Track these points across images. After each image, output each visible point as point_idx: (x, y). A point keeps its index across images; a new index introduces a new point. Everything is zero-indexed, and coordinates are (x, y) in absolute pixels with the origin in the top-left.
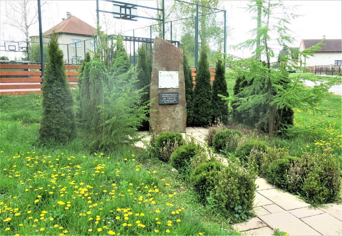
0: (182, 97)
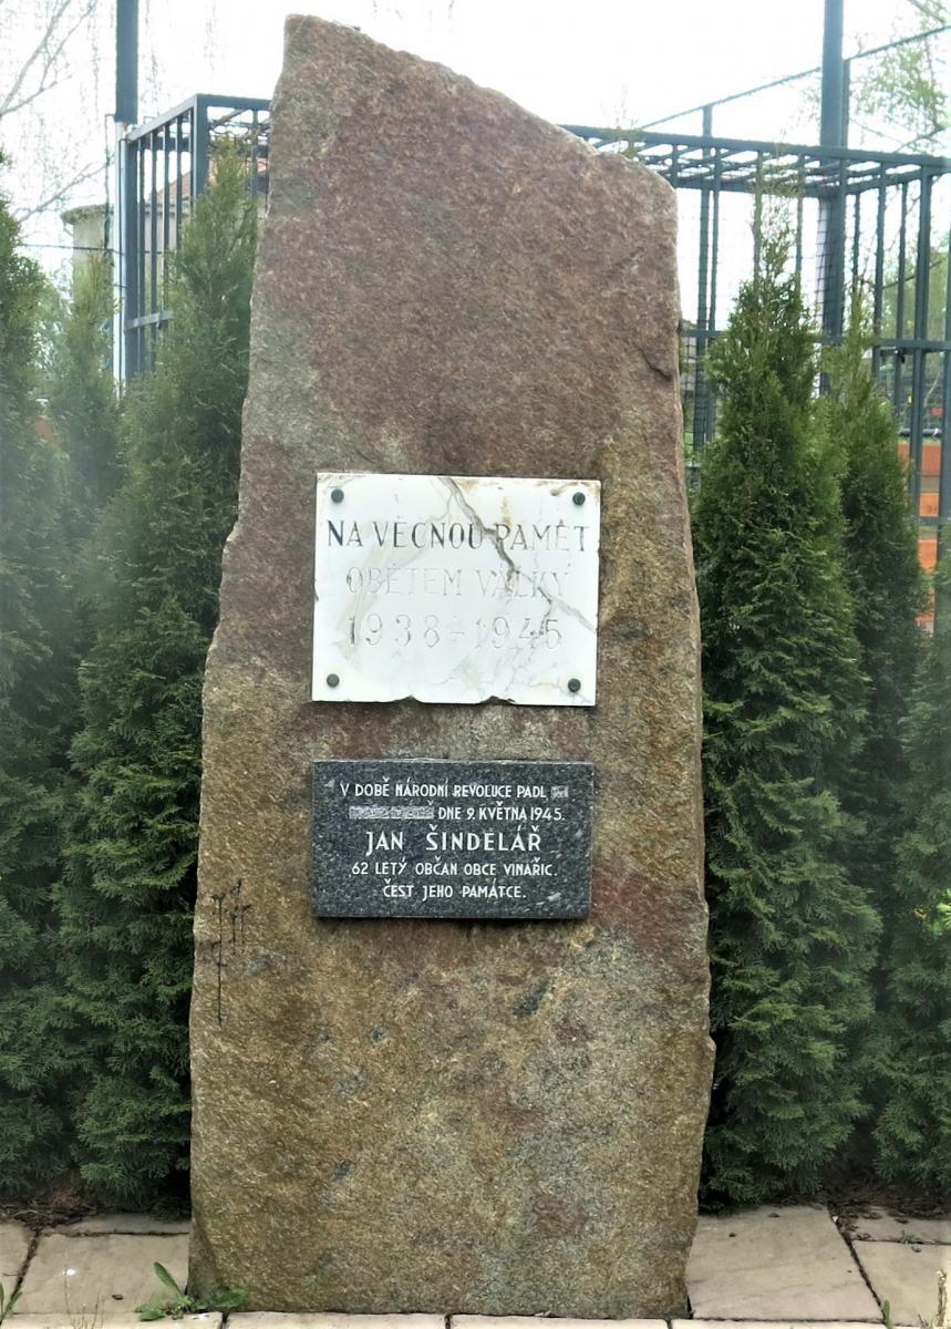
0: (650, 826)
